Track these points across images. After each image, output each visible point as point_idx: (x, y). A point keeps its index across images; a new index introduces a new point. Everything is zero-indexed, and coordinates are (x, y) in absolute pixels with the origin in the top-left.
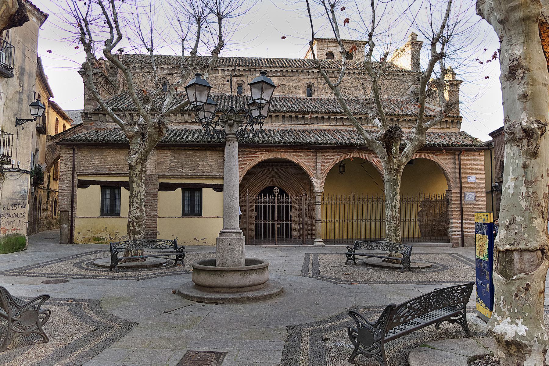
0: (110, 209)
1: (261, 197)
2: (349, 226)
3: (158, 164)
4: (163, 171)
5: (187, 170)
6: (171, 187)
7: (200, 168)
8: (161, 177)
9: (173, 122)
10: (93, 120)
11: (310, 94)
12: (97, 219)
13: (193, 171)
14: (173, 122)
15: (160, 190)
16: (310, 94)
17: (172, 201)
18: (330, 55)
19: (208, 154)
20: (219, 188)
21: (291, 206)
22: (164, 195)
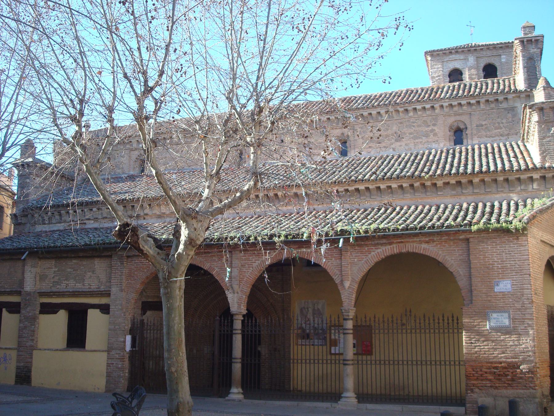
0: (76, 337)
1: (228, 320)
2: (438, 372)
3: (43, 278)
4: (45, 287)
5: (72, 285)
6: (49, 309)
7: (86, 282)
8: (42, 294)
9: (106, 218)
10: (23, 222)
11: (344, 153)
12: (62, 352)
13: (79, 287)
14: (106, 218)
15: (42, 312)
16: (344, 153)
17: (56, 326)
18: (455, 75)
19: (96, 262)
20: (105, 309)
21: (259, 335)
22: (45, 320)
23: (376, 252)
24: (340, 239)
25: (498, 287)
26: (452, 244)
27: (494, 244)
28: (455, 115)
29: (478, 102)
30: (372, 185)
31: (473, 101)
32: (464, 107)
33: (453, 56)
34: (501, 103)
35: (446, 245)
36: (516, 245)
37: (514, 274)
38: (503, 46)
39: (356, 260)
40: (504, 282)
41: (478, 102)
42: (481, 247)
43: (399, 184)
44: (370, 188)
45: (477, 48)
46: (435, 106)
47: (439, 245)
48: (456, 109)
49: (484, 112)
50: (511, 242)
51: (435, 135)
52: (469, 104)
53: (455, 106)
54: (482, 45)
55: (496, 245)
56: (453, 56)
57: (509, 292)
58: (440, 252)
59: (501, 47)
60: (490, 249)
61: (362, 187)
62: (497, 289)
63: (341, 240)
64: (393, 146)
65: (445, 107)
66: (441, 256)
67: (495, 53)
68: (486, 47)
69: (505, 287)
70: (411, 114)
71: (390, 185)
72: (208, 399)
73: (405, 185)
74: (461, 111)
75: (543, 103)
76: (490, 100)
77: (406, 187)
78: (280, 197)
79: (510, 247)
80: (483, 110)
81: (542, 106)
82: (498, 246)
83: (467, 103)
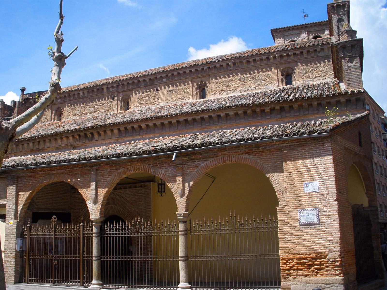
23: (205, 164)
24: (173, 154)
25: (307, 188)
26: (268, 153)
27: (303, 151)
28: (285, 63)
29: (302, 53)
30: (214, 113)
31: (298, 52)
32: (292, 57)
33: (291, 32)
34: (319, 52)
35: (264, 154)
36: (322, 151)
37: (321, 176)
38: (326, 23)
39: (188, 171)
40: (312, 184)
41: (302, 53)
42: (292, 154)
43: (235, 112)
44: (212, 116)
45: (308, 26)
46: (270, 57)
47: (257, 155)
48: (285, 58)
49: (306, 60)
50: (317, 148)
51: (271, 78)
52: (295, 54)
53: (285, 56)
54: (311, 23)
55: (305, 152)
56: (291, 32)
57: (316, 192)
58: (259, 161)
59: (325, 24)
60: (300, 155)
61: (206, 116)
62: (306, 190)
63: (175, 154)
64: (239, 89)
65: (277, 57)
66: (49, 117)
67: (320, 28)
68: (314, 25)
69: (313, 188)
70: (252, 64)
71: (228, 113)
72: (185, 275)
73: (240, 112)
74: (289, 60)
75: (346, 42)
76: (311, 50)
77: (241, 114)
78: (143, 127)
79: (317, 152)
80: (306, 58)
81: (346, 44)
82: (307, 152)
83: (293, 53)
